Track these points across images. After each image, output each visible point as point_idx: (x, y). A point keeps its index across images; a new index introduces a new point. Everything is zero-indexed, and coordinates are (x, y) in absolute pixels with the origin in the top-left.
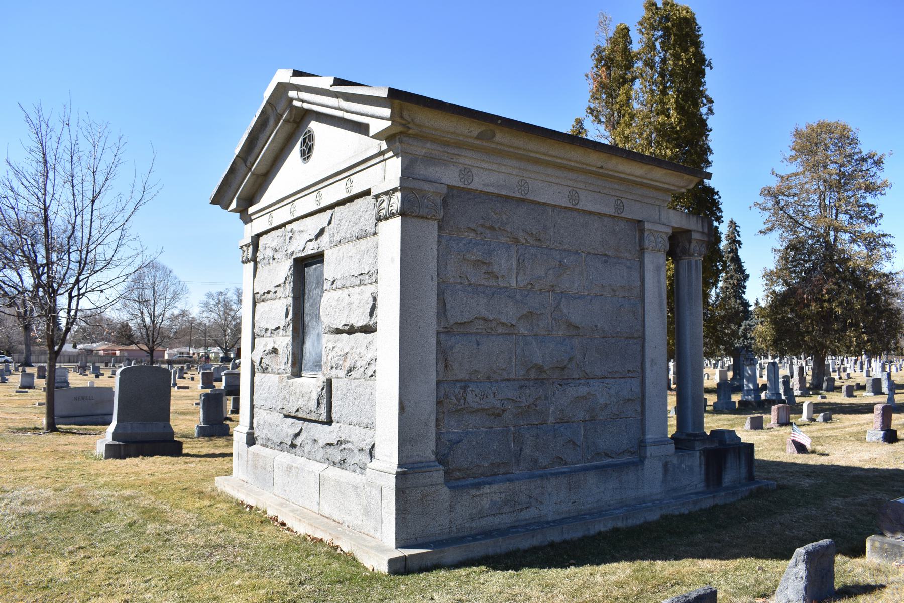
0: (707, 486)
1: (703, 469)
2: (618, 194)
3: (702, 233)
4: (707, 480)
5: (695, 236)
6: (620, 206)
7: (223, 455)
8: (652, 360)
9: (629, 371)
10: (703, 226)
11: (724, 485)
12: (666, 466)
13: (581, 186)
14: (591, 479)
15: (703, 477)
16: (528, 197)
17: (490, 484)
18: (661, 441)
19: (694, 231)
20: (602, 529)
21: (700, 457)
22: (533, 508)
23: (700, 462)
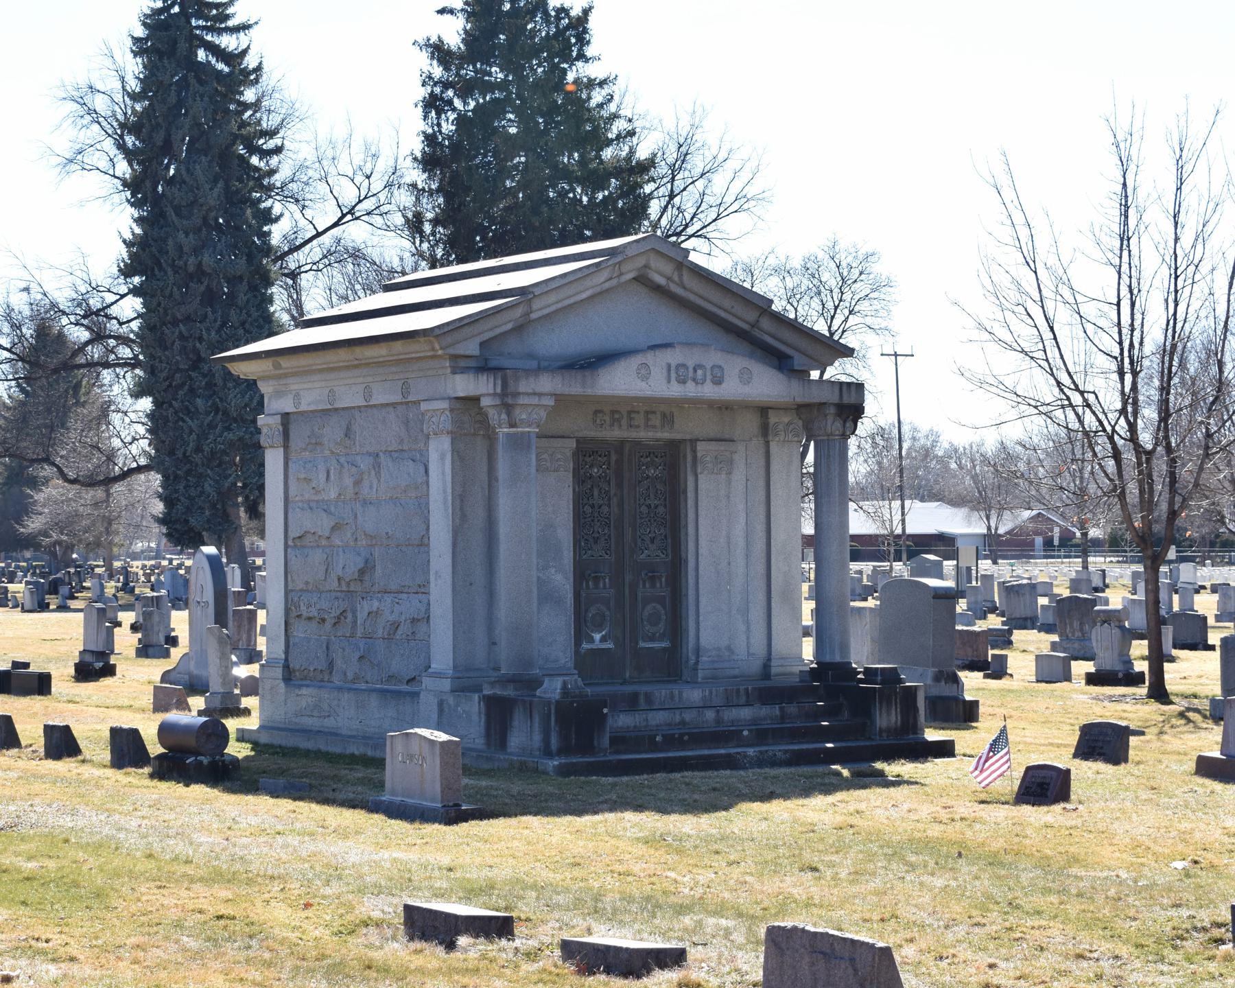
0: (488, 744)
1: (483, 720)
2: (402, 377)
3: (495, 394)
4: (488, 734)
5: (485, 402)
6: (368, 394)
7: (530, 705)
8: (437, 572)
9: (420, 586)
10: (495, 384)
11: (509, 750)
12: (441, 704)
13: (370, 379)
14: (374, 701)
15: (482, 730)
16: (336, 406)
17: (308, 686)
18: (440, 673)
19: (484, 395)
20: (356, 753)
21: (479, 703)
22: (332, 718)
23: (479, 708)
